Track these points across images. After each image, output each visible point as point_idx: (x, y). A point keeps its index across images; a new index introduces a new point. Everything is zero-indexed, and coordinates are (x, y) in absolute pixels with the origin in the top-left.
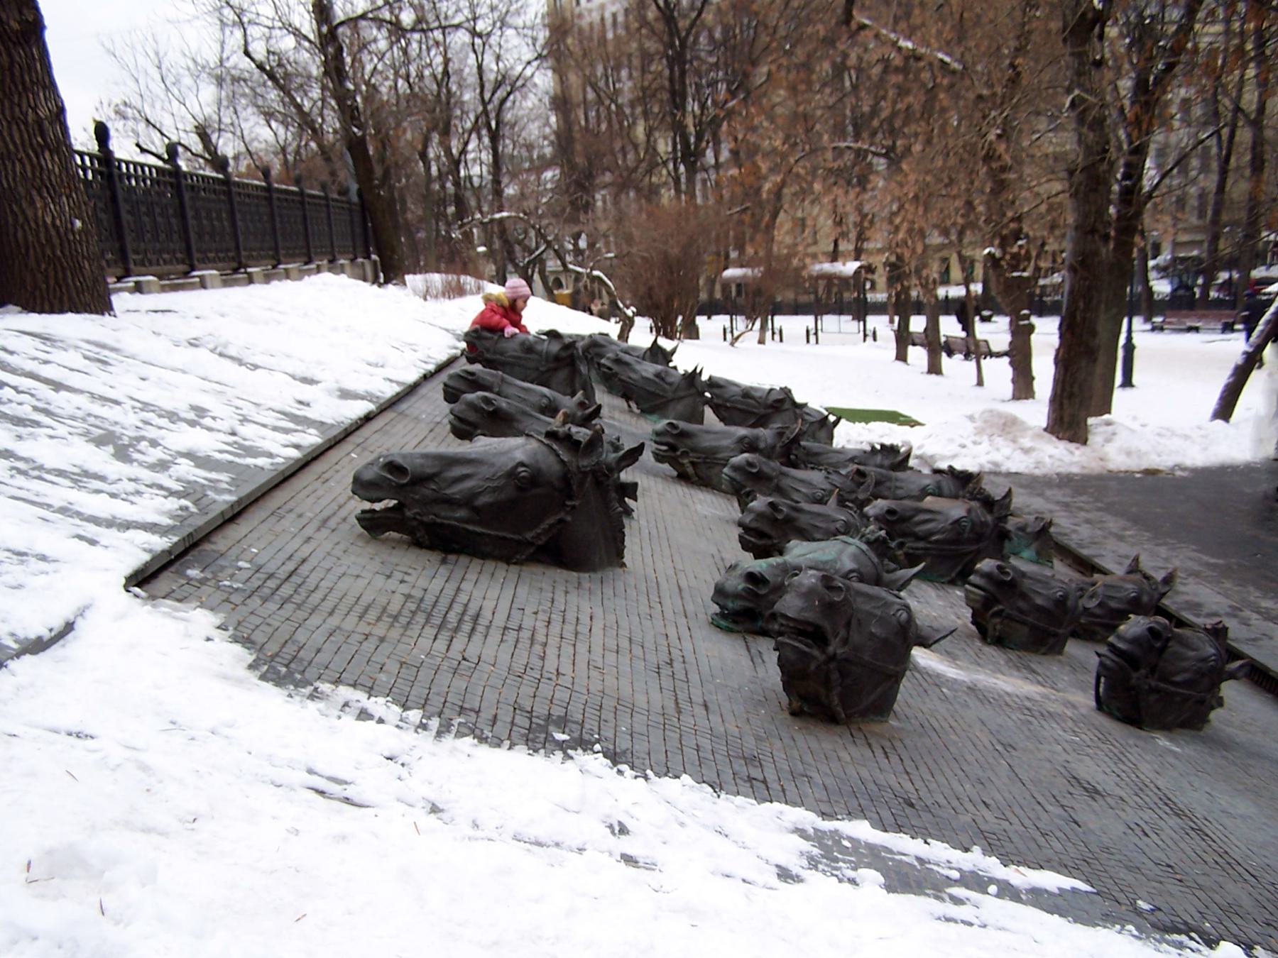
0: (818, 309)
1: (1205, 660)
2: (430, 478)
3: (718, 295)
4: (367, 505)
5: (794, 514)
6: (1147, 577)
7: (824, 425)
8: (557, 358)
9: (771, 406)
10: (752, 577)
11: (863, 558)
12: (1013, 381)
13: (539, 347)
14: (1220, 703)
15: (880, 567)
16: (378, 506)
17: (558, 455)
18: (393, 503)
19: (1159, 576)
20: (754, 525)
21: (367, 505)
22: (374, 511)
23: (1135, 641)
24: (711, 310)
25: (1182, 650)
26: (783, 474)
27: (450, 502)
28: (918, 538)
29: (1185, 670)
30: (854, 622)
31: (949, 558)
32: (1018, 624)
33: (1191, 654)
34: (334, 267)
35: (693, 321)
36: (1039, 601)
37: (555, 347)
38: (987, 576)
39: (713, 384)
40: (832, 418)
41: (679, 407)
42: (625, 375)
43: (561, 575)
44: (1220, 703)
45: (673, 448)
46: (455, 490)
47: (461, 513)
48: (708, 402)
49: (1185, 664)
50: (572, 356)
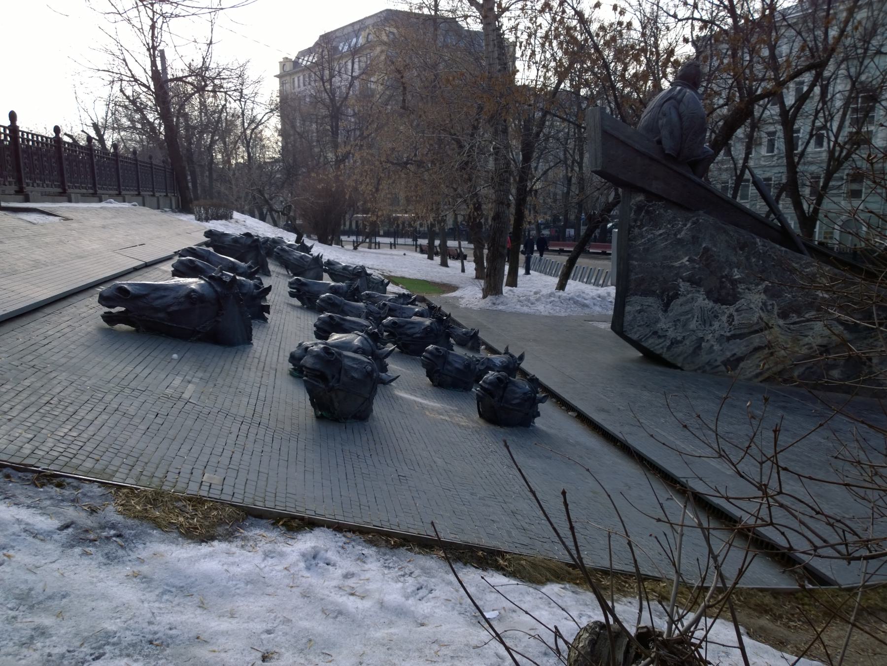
0: (395, 234)
1: (525, 394)
2: (144, 296)
3: (354, 226)
4: (107, 310)
5: (342, 322)
6: (512, 356)
7: (381, 285)
8: (250, 246)
9: (355, 275)
10: (498, 378)
11: (365, 342)
12: (476, 269)
13: (241, 241)
14: (538, 415)
15: (375, 348)
16: (114, 310)
17: (214, 288)
18: (123, 309)
19: (517, 355)
20: (322, 326)
21: (107, 310)
22: (111, 313)
23: (491, 383)
24: (348, 233)
25: (514, 388)
26: (345, 304)
27: (157, 310)
28: (408, 336)
29: (516, 398)
30: (343, 372)
31: (410, 346)
32: (447, 379)
33: (519, 390)
34: (120, 196)
35: (295, 233)
36: (457, 365)
37: (249, 242)
38: (430, 352)
39: (329, 263)
40: (386, 281)
41: (312, 273)
42: (286, 256)
43: (217, 347)
44: (538, 415)
45: (298, 291)
46: (408, 332)
47: (161, 315)
48: (326, 271)
49: (517, 396)
50: (257, 246)
